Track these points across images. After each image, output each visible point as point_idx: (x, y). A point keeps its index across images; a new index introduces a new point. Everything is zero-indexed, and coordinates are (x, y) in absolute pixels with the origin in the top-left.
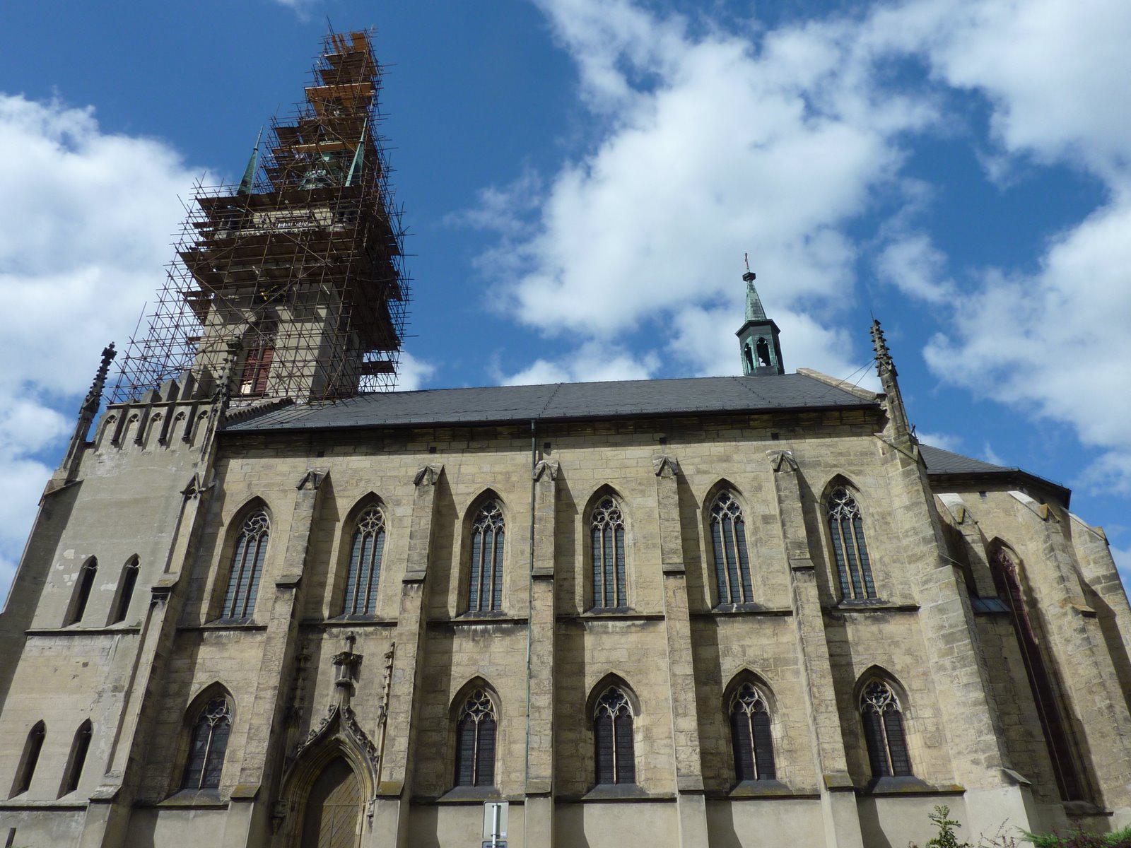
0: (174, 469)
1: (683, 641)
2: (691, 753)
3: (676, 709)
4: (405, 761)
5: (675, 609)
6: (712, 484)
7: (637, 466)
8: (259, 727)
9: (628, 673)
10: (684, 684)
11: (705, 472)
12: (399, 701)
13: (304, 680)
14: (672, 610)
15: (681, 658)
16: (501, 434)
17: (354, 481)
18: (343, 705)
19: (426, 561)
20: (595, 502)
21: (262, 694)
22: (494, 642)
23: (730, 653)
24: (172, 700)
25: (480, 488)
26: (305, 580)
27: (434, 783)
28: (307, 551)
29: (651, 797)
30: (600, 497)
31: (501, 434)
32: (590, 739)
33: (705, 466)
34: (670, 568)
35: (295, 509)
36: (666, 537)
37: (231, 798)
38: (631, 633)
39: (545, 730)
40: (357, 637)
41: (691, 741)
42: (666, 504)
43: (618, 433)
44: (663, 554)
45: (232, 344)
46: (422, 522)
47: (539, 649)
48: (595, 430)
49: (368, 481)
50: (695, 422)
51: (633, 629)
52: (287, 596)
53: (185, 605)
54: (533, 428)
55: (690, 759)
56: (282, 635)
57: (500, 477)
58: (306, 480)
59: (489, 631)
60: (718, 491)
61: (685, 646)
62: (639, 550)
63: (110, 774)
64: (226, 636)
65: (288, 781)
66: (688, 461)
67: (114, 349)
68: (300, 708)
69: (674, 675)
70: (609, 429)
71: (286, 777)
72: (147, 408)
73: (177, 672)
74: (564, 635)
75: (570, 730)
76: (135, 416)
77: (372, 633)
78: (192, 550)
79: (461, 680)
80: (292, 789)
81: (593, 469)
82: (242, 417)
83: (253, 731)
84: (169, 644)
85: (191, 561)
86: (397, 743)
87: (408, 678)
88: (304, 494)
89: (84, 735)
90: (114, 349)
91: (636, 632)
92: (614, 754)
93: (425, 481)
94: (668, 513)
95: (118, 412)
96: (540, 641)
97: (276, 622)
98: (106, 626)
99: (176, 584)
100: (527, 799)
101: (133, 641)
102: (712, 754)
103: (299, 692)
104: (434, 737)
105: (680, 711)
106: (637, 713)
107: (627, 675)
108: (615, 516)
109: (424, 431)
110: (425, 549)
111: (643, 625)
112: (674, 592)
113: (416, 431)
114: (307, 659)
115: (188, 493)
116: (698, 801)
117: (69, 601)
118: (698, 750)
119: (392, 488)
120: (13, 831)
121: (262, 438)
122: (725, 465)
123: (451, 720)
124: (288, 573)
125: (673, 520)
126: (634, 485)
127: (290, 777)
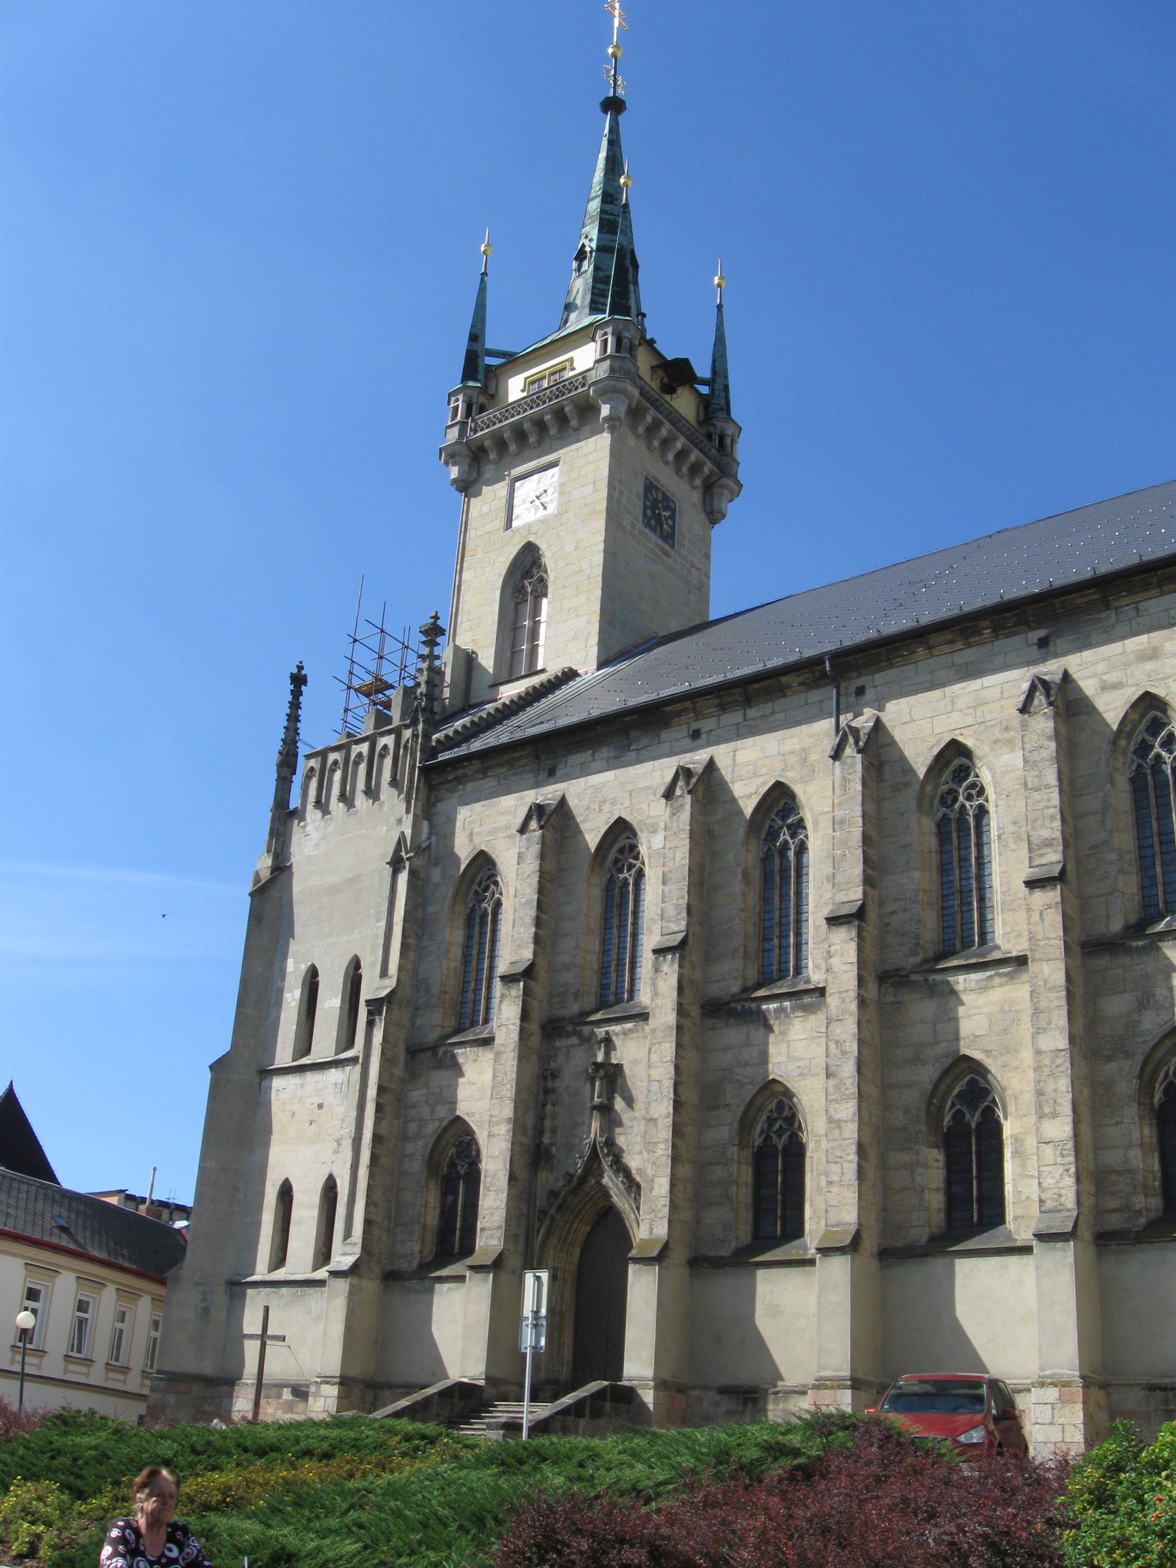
0: (385, 828)
1: (1053, 995)
2: (1061, 1175)
3: (1041, 1106)
4: (666, 1210)
5: (1042, 943)
6: (1127, 707)
7: (1002, 698)
8: (495, 1175)
9: (988, 1052)
10: (1054, 1066)
11: (1116, 686)
12: (656, 1126)
13: (554, 1105)
14: (1037, 945)
15: (1049, 1023)
16: (789, 687)
17: (596, 806)
18: (601, 1136)
19: (685, 914)
20: (940, 775)
21: (495, 1130)
22: (794, 1025)
23: (1151, 1002)
24: (412, 1144)
25: (765, 783)
26: (542, 964)
27: (721, 1237)
28: (538, 922)
29: (1018, 1244)
30: (949, 763)
31: (789, 687)
32: (937, 1161)
33: (1114, 674)
34: (1038, 873)
35: (519, 864)
36: (1035, 820)
37: (817, 1249)
38: (993, 987)
39: (848, 1154)
40: (614, 1038)
41: (1063, 1156)
42: (1035, 762)
43: (969, 646)
44: (1030, 850)
45: (426, 630)
46: (677, 855)
47: (838, 1031)
48: (930, 648)
49: (614, 802)
50: (1094, 597)
51: (997, 980)
52: (514, 993)
53: (414, 1016)
54: (828, 669)
55: (1061, 1185)
56: (512, 1046)
57: (792, 760)
58: (528, 818)
59: (787, 1008)
60: (1143, 716)
61: (1056, 1003)
62: (1006, 846)
63: (348, 1241)
64: (462, 1054)
65: (544, 1242)
66: (1086, 672)
67: (303, 672)
68: (552, 1144)
69: (1038, 1052)
70: (952, 642)
71: (540, 1236)
72: (372, 740)
73: (413, 1107)
74: (892, 1003)
75: (902, 1149)
76: (336, 762)
77: (631, 1030)
78: (412, 941)
79: (750, 1087)
80: (551, 1252)
81: (931, 718)
82: (450, 743)
83: (489, 1179)
84: (399, 1071)
85: (412, 955)
86: (656, 1186)
87: (665, 1093)
88: (528, 839)
89: (330, 1189)
90: (303, 672)
91: (1002, 985)
92: (975, 1182)
93: (678, 792)
94: (1039, 776)
95: (317, 761)
96: (839, 1020)
97: (504, 1029)
98: (336, 1055)
99: (393, 992)
100: (818, 1256)
101: (356, 1071)
102: (1117, 1172)
103: (548, 1123)
104: (718, 1172)
105: (1047, 1110)
106: (1006, 1118)
107: (987, 1057)
108: (974, 792)
109: (678, 707)
110: (683, 897)
111: (1013, 972)
112: (1041, 915)
113: (667, 709)
114: (554, 1075)
115: (396, 864)
116: (1064, 1250)
117: (295, 1027)
118: (1073, 1170)
119: (644, 806)
120: (267, 1309)
121: (477, 764)
122: (1149, 666)
123: (742, 1146)
124: (517, 958)
125: (1047, 787)
126: (997, 733)
127: (548, 1234)
